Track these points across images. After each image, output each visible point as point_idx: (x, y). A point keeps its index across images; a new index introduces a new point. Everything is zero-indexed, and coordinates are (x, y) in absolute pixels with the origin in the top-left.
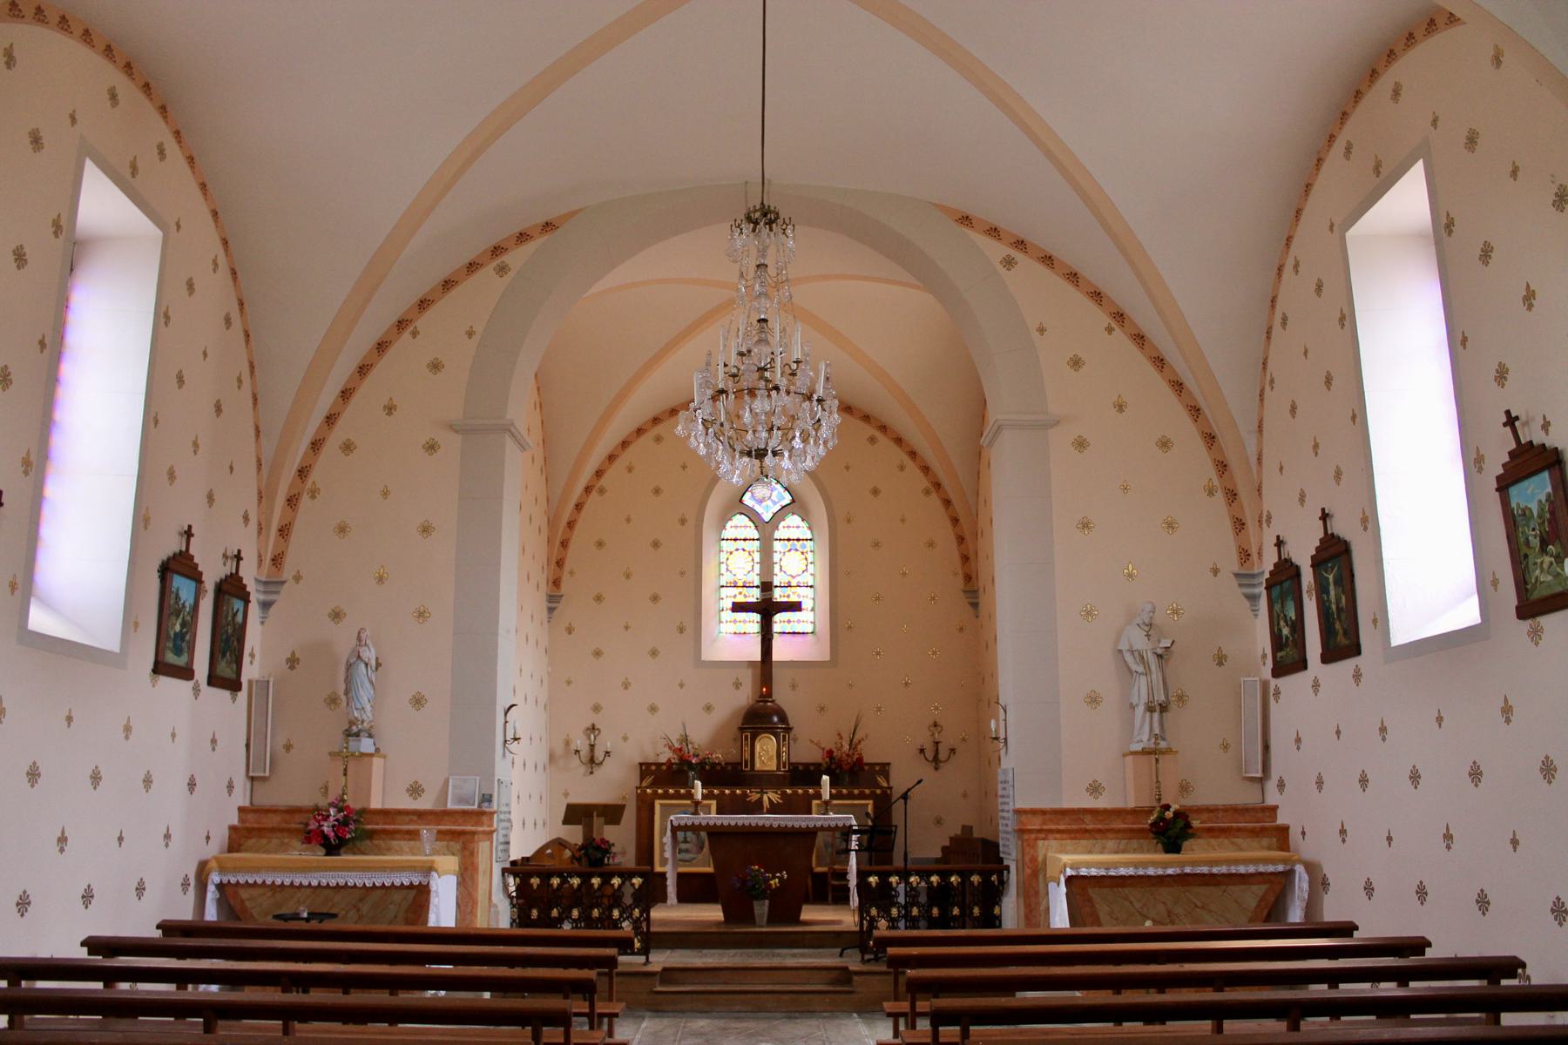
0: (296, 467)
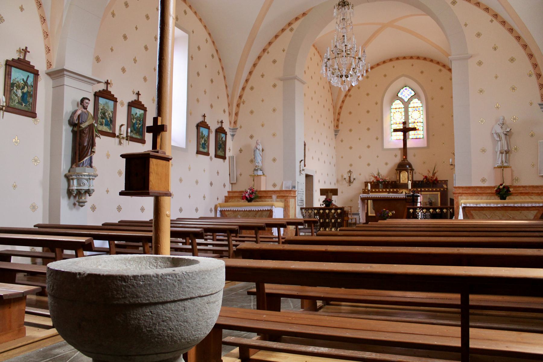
0: (238, 96)
